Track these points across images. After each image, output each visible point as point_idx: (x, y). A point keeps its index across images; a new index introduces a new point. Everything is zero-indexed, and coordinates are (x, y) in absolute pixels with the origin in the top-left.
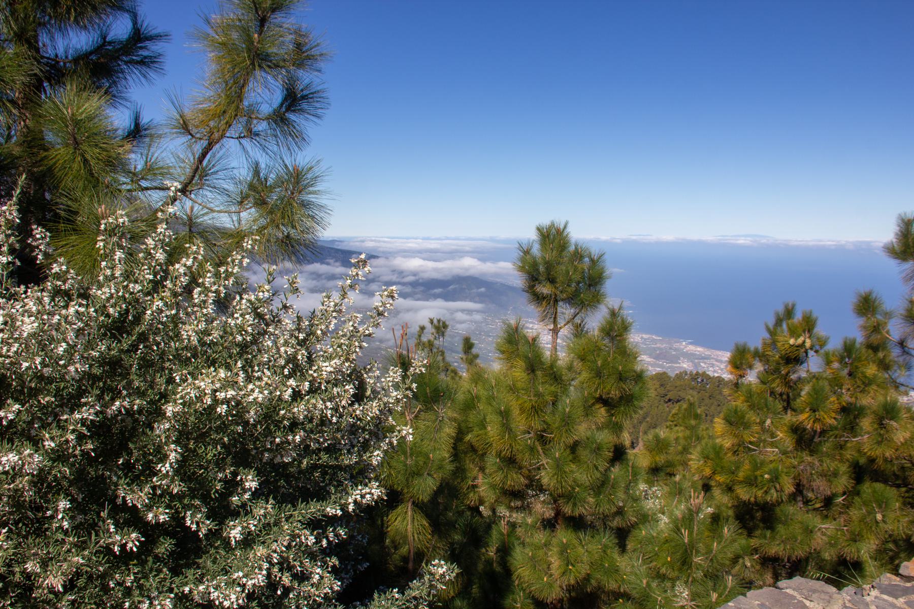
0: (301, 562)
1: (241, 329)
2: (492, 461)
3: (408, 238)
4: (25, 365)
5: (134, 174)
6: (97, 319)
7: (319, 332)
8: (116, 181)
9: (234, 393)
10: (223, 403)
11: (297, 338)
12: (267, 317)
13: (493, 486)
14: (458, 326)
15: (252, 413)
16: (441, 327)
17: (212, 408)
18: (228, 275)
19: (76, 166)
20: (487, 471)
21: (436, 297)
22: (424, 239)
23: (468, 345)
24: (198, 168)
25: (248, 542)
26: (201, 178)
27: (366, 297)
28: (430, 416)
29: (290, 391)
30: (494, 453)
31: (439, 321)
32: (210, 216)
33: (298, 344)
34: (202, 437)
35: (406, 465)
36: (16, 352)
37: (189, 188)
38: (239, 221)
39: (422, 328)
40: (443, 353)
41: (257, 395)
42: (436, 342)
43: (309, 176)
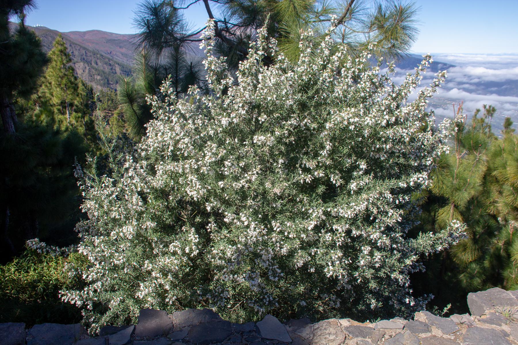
0: (383, 206)
1: (364, 90)
2: (507, 188)
3: (476, 54)
4: (269, 98)
5: (317, 13)
6: (297, 82)
7: (403, 94)
8: (308, 16)
9: (358, 119)
10: (352, 125)
11: (392, 96)
12: (377, 84)
13: (506, 204)
14: (505, 112)
15: (366, 131)
16: (491, 111)
17: (347, 127)
18: (360, 63)
19: (290, 10)
20: (504, 194)
21: (492, 93)
22: (488, 55)
23: (508, 123)
24: (349, 9)
25: (359, 191)
26: (350, 14)
27: (445, 91)
28: (472, 157)
29: (385, 121)
30: (509, 183)
31: (490, 107)
32: (354, 34)
33: (392, 99)
34: (342, 142)
35: (452, 183)
36: (266, 93)
37: (344, 20)
38: (369, 37)
39: (478, 111)
40: (490, 127)
41: (369, 121)
42: (486, 120)
43: (408, 12)
